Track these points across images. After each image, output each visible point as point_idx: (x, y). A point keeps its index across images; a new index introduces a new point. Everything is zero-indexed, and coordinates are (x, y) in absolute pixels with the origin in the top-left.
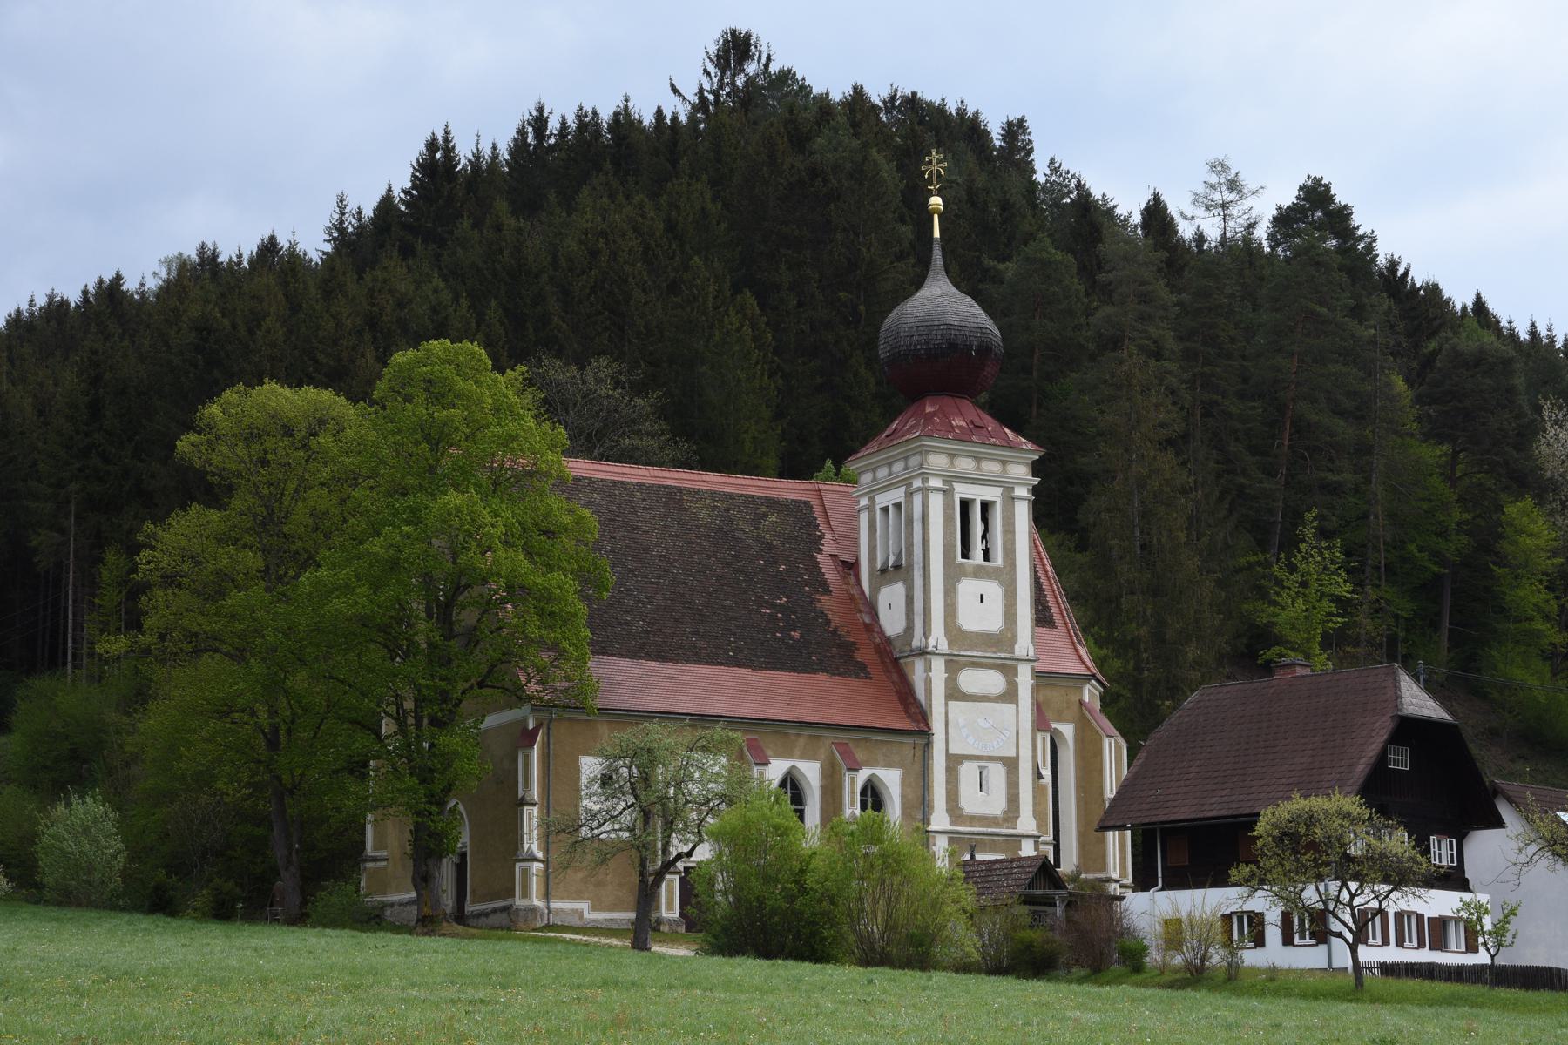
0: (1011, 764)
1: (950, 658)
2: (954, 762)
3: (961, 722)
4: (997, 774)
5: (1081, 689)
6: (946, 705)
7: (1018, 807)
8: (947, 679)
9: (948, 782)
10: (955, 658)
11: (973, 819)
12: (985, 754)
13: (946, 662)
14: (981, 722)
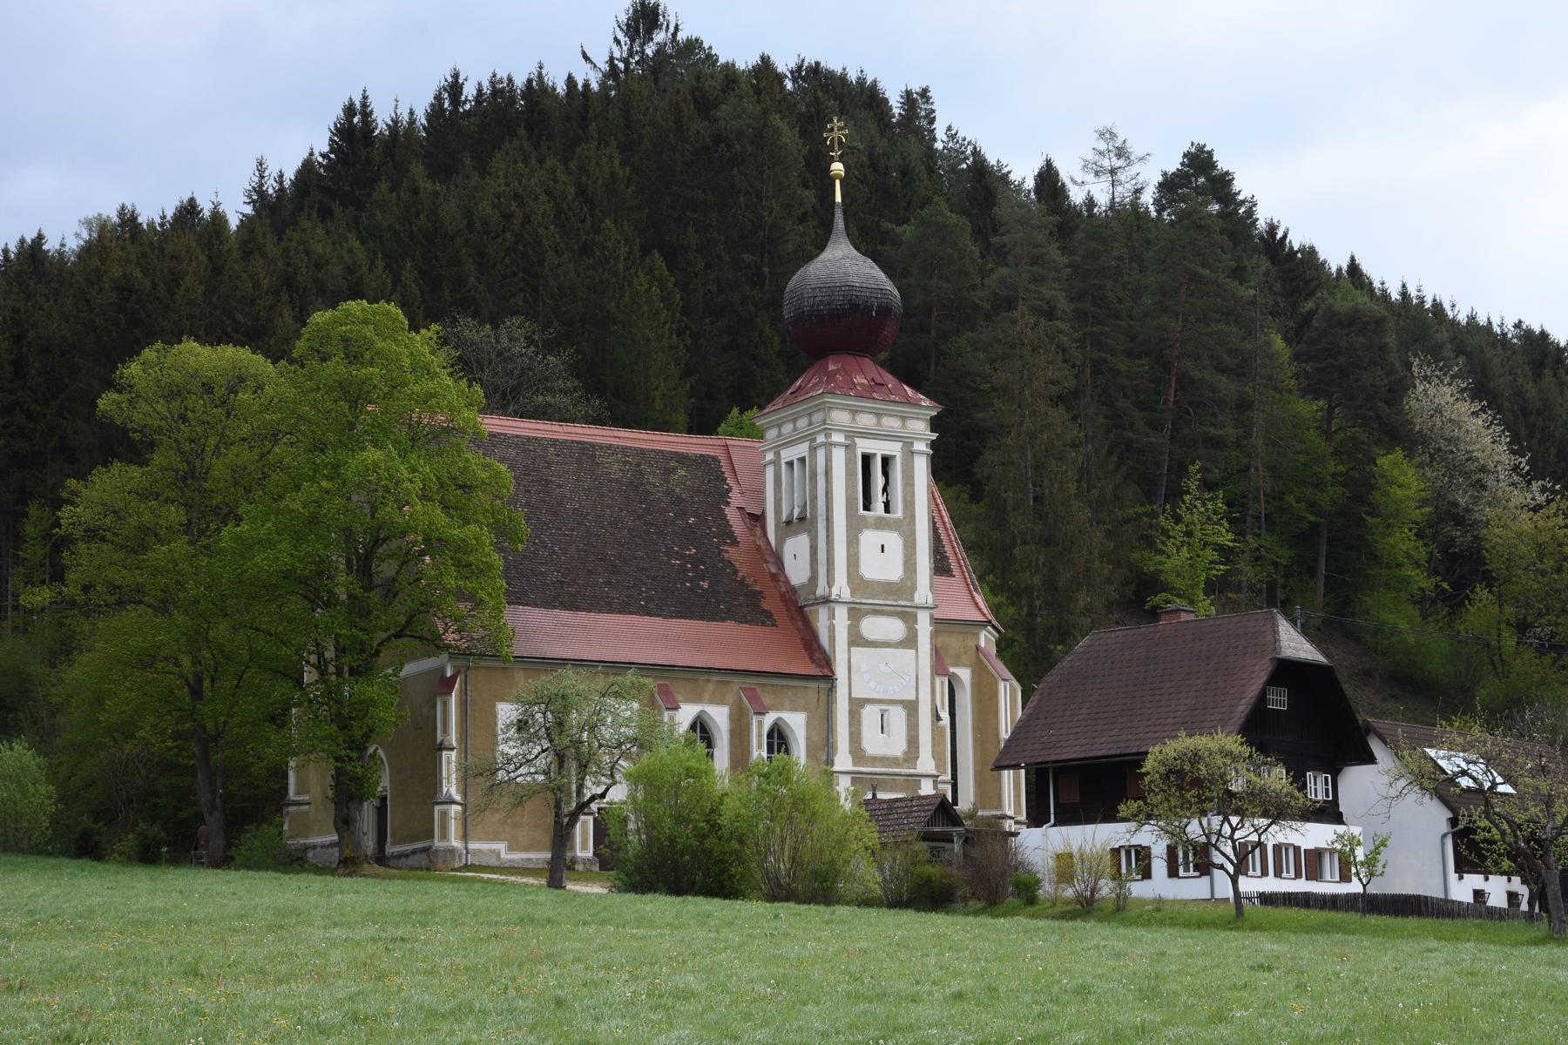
0: (911, 707)
1: (853, 606)
2: (856, 705)
3: (864, 667)
4: (898, 716)
5: (977, 635)
6: (849, 651)
7: (918, 748)
8: (849, 625)
9: (851, 725)
10: (857, 606)
11: (875, 760)
12: (887, 698)
13: (850, 610)
14: (884, 668)
